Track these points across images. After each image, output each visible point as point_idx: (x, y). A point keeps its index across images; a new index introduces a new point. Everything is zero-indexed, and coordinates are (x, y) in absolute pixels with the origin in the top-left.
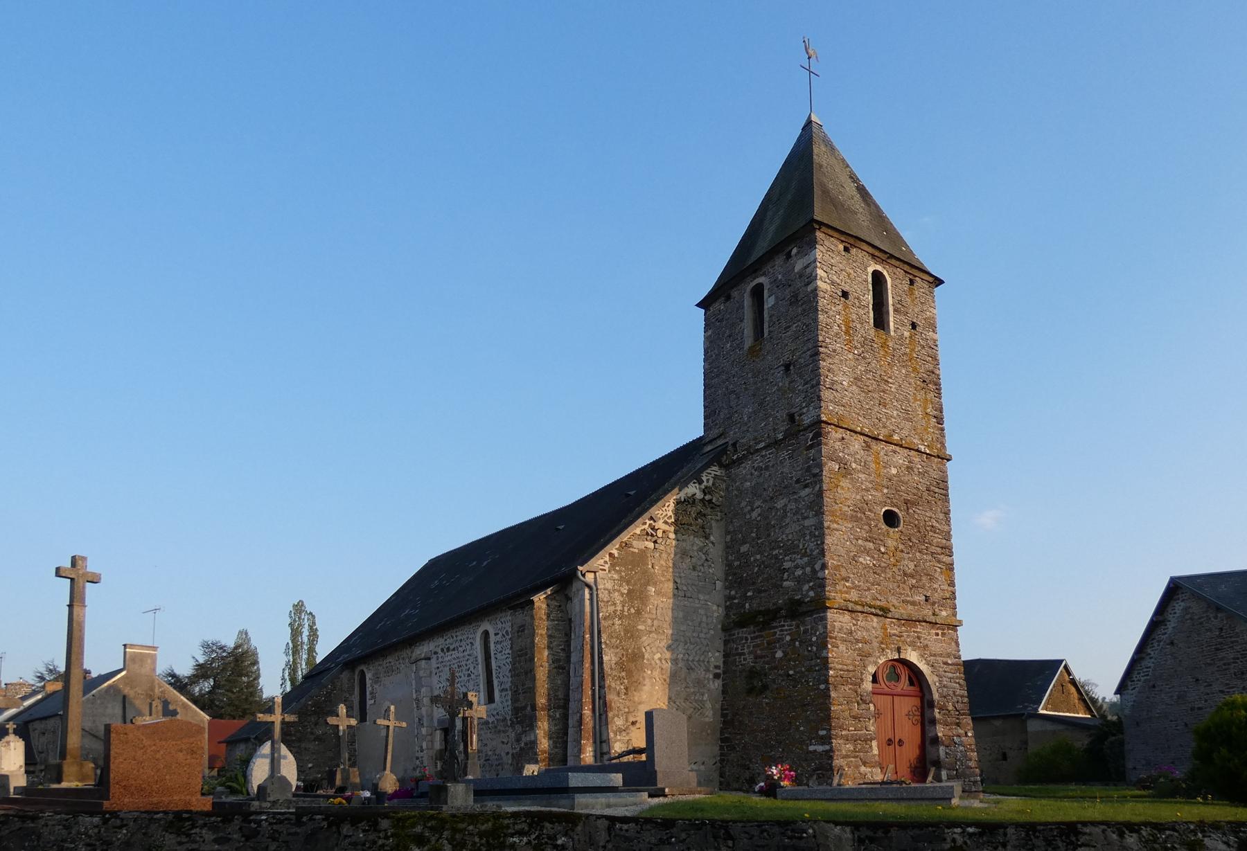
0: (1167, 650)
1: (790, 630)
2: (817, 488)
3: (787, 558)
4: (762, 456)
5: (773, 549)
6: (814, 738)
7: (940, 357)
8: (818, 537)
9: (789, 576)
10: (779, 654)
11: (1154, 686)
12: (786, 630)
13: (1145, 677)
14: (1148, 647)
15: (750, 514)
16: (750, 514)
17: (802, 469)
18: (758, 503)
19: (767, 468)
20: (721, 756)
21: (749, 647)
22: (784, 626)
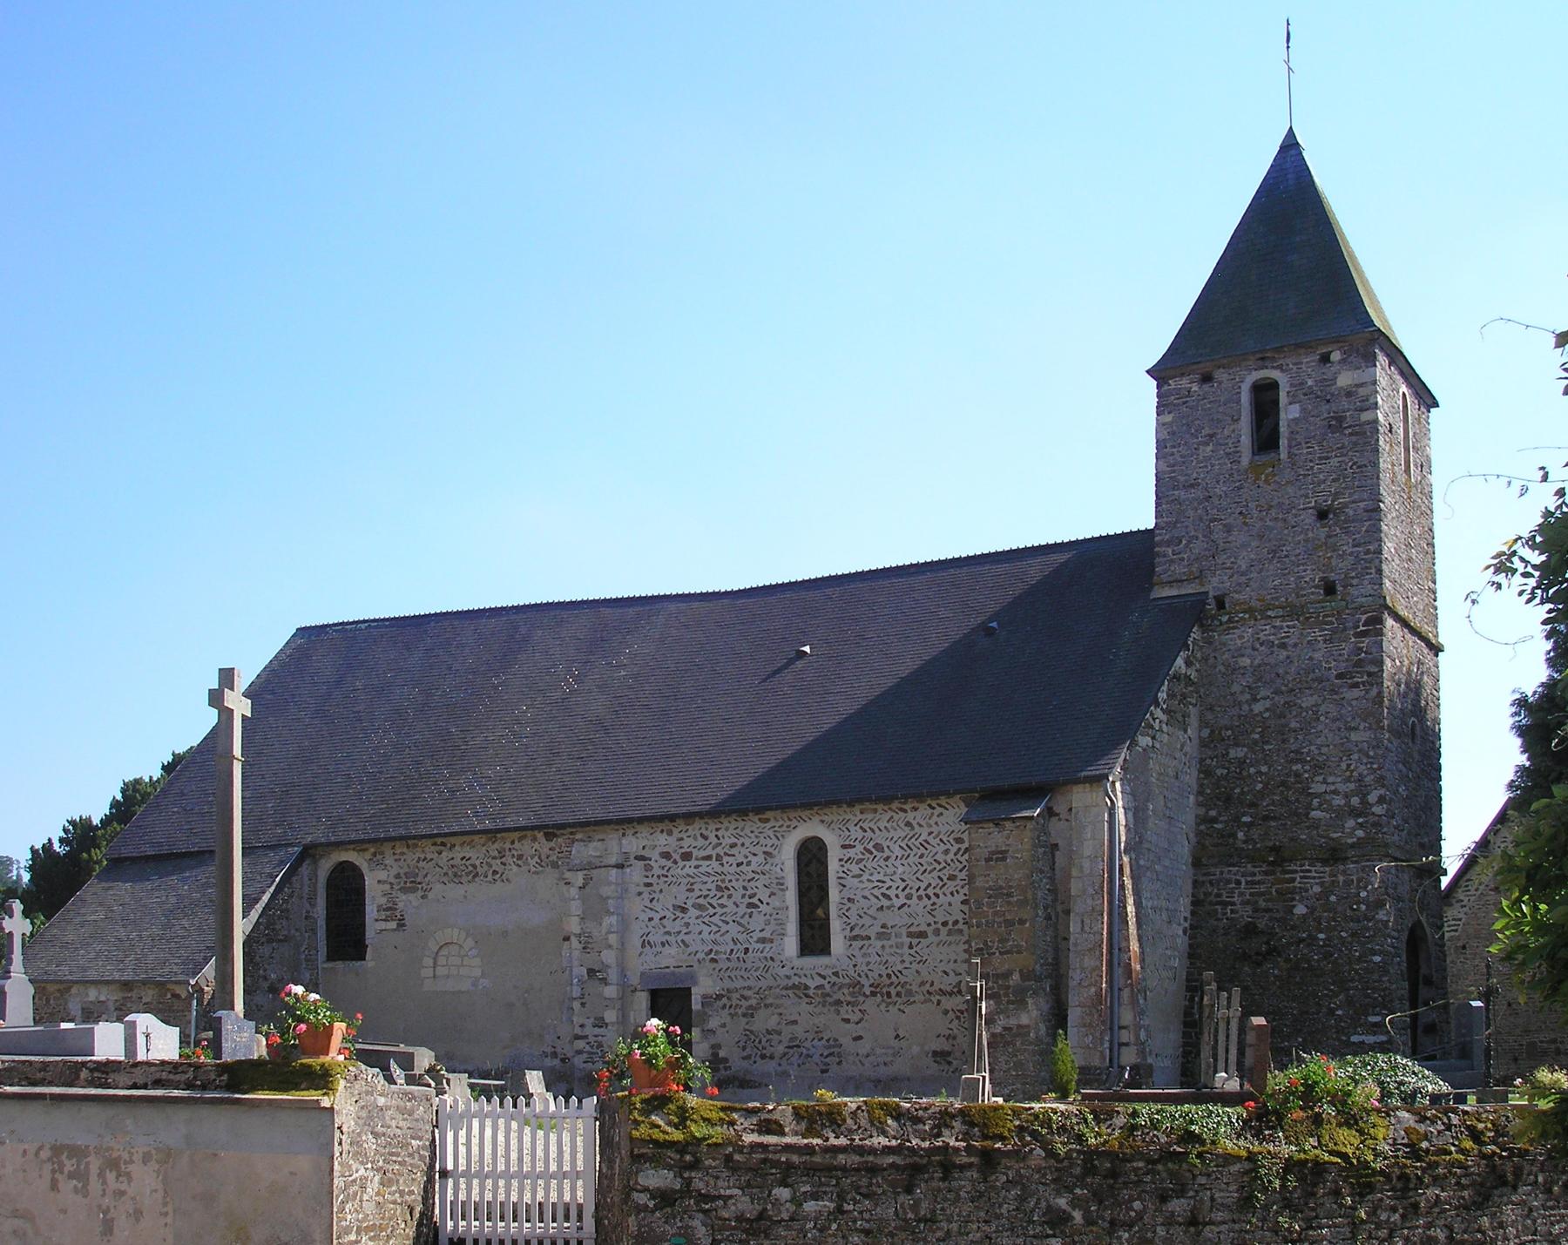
0: (1488, 898)
1: (1320, 878)
2: (1374, 692)
3: (1317, 779)
4: (1274, 627)
5: (1292, 761)
6: (1361, 1026)
7: (1434, 510)
8: (1372, 757)
9: (1321, 804)
10: (1300, 910)
11: (1464, 947)
12: (1314, 878)
13: (1453, 934)
14: (1460, 891)
15: (1250, 705)
16: (1250, 705)
17: (1347, 660)
18: (1263, 693)
19: (1283, 646)
20: (1183, 1046)
21: (1241, 894)
22: (1310, 871)
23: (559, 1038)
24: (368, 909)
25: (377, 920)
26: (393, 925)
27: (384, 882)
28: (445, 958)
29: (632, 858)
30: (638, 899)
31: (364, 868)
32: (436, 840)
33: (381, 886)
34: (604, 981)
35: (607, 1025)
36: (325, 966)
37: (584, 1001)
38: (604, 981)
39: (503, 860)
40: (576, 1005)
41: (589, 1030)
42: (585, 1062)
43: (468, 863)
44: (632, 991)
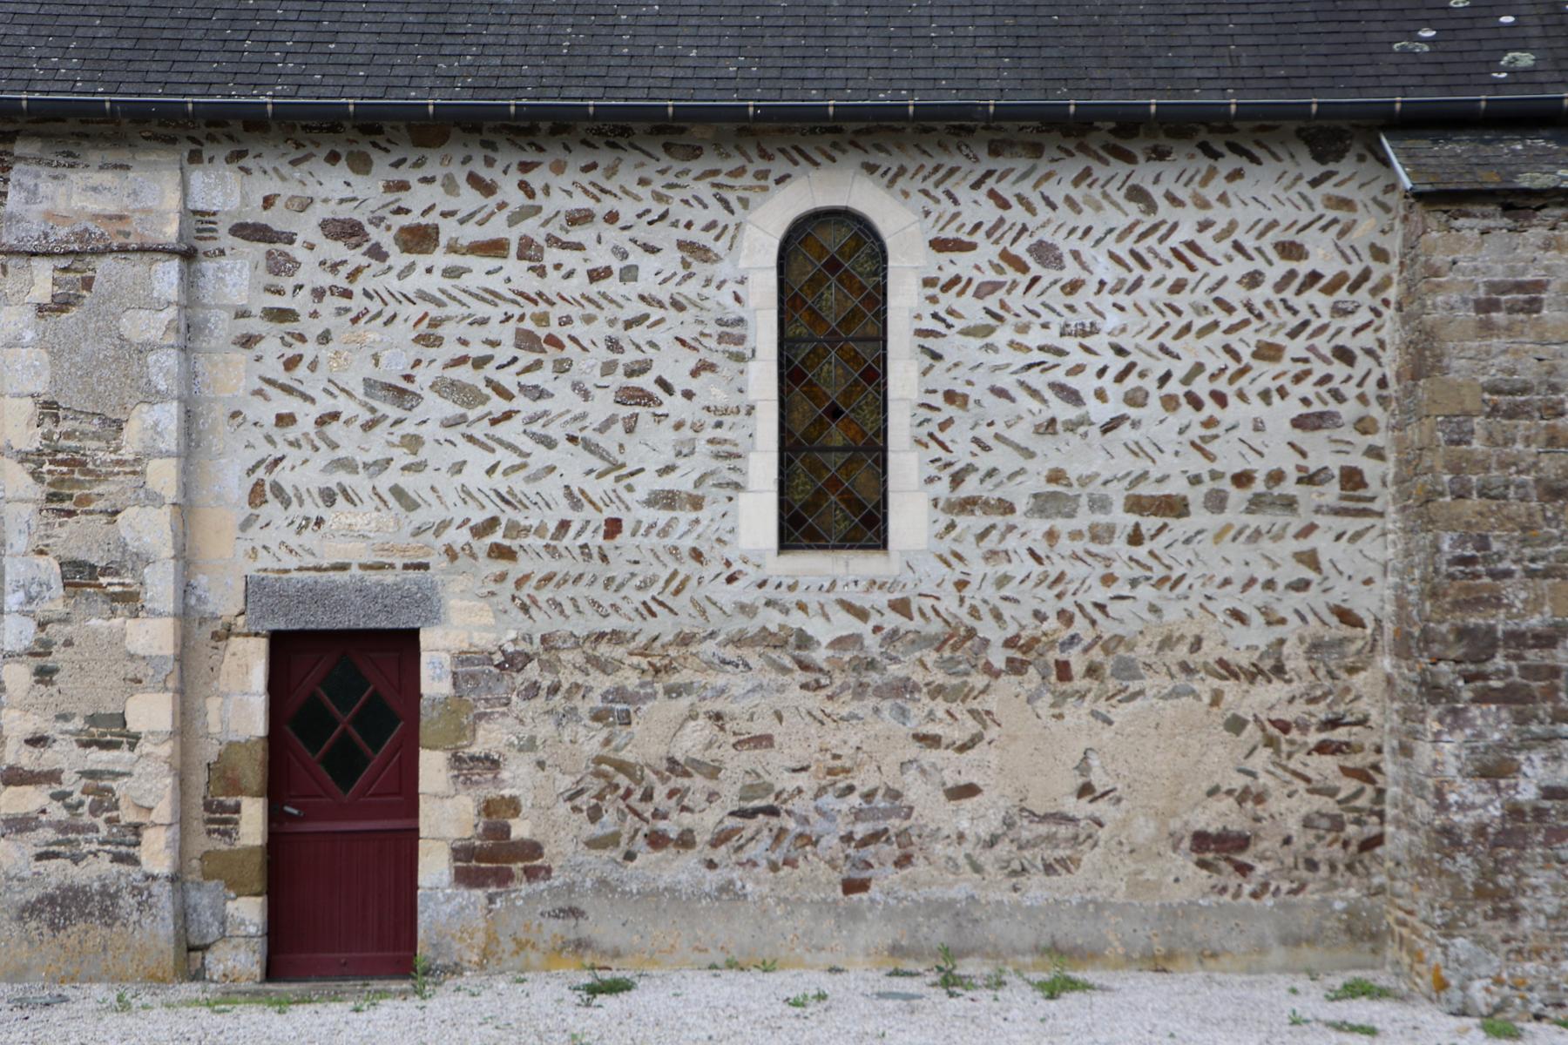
34: (129, 600)
37: (49, 662)
38: (129, 600)
41: (66, 756)
44: (215, 636)
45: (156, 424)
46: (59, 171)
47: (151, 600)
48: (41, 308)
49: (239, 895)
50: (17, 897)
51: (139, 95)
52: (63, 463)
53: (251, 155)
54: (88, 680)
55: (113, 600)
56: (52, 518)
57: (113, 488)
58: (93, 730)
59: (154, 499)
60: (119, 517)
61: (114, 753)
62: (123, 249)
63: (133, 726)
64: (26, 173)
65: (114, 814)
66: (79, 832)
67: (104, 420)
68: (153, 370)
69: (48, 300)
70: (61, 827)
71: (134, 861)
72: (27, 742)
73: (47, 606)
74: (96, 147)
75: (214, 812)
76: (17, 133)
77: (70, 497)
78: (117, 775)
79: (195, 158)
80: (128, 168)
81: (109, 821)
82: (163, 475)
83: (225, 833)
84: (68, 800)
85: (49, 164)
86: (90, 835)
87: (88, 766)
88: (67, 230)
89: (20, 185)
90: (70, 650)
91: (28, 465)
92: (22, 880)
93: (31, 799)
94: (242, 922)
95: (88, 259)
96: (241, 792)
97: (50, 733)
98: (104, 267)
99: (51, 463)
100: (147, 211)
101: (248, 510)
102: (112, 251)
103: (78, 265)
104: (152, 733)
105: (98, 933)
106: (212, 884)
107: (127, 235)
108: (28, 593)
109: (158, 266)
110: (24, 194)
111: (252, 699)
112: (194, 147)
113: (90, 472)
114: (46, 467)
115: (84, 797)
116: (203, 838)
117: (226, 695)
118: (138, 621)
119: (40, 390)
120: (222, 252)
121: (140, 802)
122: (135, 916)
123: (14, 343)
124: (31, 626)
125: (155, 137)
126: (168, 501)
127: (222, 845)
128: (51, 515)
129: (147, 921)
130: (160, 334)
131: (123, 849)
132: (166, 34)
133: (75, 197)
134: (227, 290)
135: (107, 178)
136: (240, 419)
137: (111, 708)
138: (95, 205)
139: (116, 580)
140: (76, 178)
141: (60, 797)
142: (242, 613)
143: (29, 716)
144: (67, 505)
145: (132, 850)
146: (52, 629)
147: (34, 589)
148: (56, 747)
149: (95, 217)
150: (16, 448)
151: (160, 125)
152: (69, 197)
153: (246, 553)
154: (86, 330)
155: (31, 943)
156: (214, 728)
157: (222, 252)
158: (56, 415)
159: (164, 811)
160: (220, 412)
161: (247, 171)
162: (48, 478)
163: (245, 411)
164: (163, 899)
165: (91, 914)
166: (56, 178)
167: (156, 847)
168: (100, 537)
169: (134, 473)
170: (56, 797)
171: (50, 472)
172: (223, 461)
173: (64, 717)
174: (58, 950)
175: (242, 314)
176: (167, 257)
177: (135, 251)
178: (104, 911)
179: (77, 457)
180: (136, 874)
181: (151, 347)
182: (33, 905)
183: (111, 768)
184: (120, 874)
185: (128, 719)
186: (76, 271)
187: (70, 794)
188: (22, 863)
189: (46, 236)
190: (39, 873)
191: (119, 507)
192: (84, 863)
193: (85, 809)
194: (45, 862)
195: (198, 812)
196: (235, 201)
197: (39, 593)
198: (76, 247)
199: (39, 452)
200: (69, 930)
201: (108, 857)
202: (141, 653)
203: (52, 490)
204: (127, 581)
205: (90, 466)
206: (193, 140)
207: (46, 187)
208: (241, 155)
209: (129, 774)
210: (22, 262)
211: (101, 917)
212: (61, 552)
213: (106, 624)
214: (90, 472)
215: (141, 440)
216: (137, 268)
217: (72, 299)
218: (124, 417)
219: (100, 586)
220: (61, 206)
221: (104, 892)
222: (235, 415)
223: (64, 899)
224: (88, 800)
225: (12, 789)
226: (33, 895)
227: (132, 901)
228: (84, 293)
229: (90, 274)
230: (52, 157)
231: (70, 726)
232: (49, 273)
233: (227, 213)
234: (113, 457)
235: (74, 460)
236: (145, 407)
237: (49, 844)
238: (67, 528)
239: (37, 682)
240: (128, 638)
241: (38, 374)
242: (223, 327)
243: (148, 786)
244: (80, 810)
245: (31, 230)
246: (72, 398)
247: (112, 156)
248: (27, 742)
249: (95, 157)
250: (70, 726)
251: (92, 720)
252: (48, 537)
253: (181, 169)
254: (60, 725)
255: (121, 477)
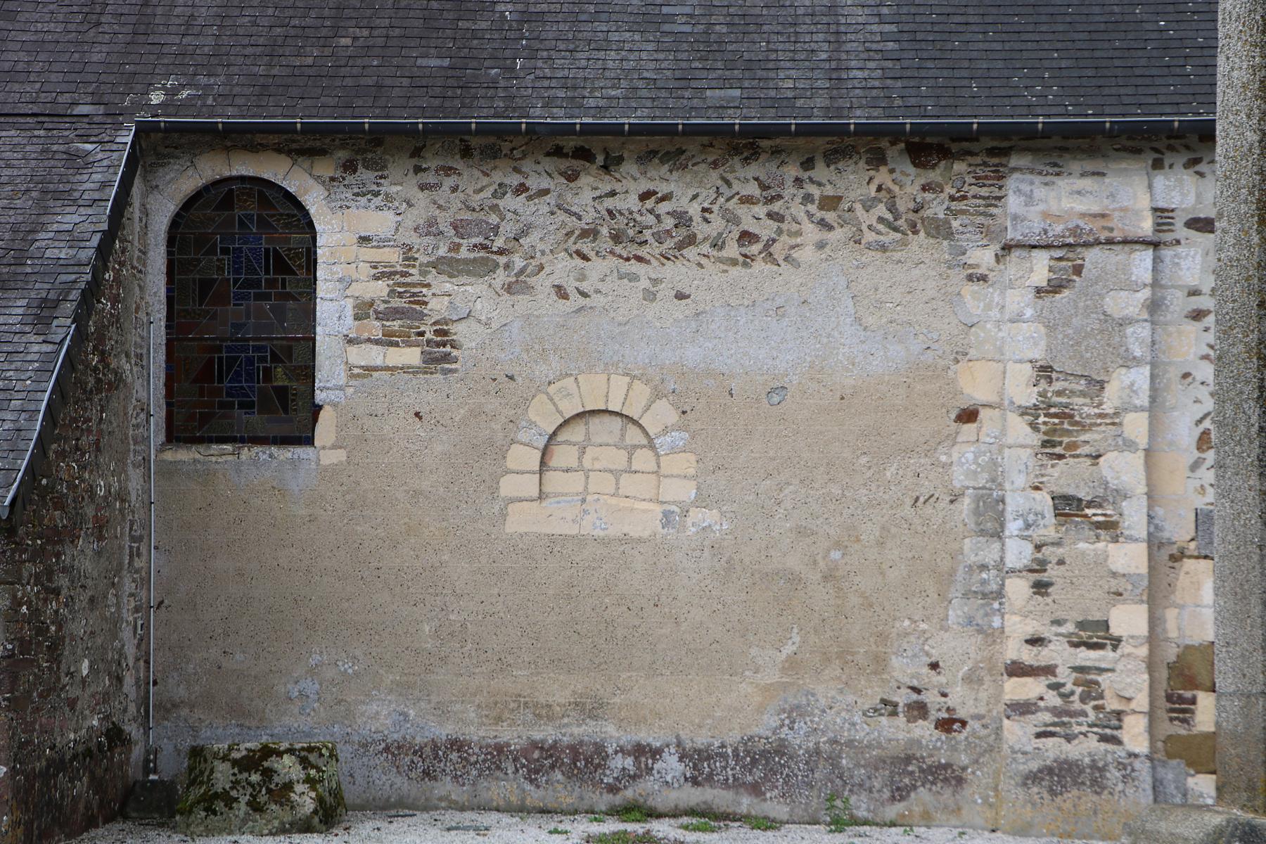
23: (934, 666)
24: (324, 310)
25: (351, 341)
26: (411, 356)
27: (383, 243)
28: (574, 451)
29: (1179, 223)
30: (1193, 328)
31: (314, 200)
32: (561, 141)
33: (369, 254)
34: (1110, 527)
35: (1116, 642)
36: (169, 456)
37: (1044, 577)
38: (1110, 527)
39: (776, 207)
40: (1018, 589)
41: (1059, 654)
42: (1039, 735)
43: (664, 208)
44: (1173, 558)
45: (1132, 384)
46: (1049, 178)
47: (1129, 528)
48: (1039, 291)
49: (1198, 772)
50: (1021, 767)
51: (1124, 115)
52: (1055, 415)
53: (1206, 160)
54: (1077, 593)
55: (1097, 528)
56: (1045, 461)
57: (1096, 436)
58: (1082, 633)
59: (1130, 445)
60: (1101, 460)
61: (1100, 653)
62: (1110, 242)
63: (1115, 630)
64: (1022, 181)
65: (1100, 702)
66: (1071, 717)
67: (1089, 380)
68: (1131, 340)
69: (1045, 284)
70: (1055, 711)
71: (1116, 741)
72: (1027, 641)
73: (1042, 531)
74: (1075, 158)
75: (1174, 703)
76: (1011, 148)
77: (1060, 443)
78: (1101, 671)
79: (1158, 165)
80: (1104, 175)
81: (1096, 708)
82: (1136, 426)
83: (1184, 721)
84: (1062, 690)
85: (1040, 173)
86: (1081, 719)
87: (1078, 663)
88: (1061, 227)
89: (1019, 191)
90: (1062, 567)
91: (1027, 417)
92: (1025, 753)
93: (1030, 688)
94: (1201, 795)
95: (1079, 250)
96: (1197, 687)
97: (1046, 635)
98: (1092, 257)
99: (1046, 415)
100: (1124, 209)
101: (1196, 454)
102: (1101, 243)
103: (1071, 255)
104: (1132, 637)
105: (1089, 799)
106: (1174, 762)
107: (1111, 230)
108: (1026, 521)
109: (1137, 255)
110: (1022, 198)
111: (1204, 610)
112: (1157, 156)
113: (1077, 423)
114: (1042, 419)
115: (1075, 688)
116: (1167, 724)
117: (1181, 607)
118: (1118, 545)
119: (1037, 357)
120: (1178, 242)
121: (1122, 694)
122: (1120, 786)
123: (1017, 319)
124: (1028, 549)
125: (1125, 149)
126: (1142, 447)
127: (1180, 730)
128: (1045, 458)
129: (1130, 791)
130: (1137, 310)
131: (1108, 731)
132: (1117, 63)
133: (1064, 200)
134: (1181, 273)
135: (1087, 183)
136: (1190, 379)
137: (1097, 616)
138: (1081, 205)
139: (1099, 511)
140: (1063, 184)
141: (1055, 687)
142: (1192, 540)
143: (1028, 621)
144: (1058, 450)
145: (1115, 733)
146: (1046, 551)
147: (1031, 518)
148: (1051, 646)
149: (1083, 215)
150: (1018, 403)
151: (1129, 138)
152: (1060, 200)
153: (1196, 490)
154: (1076, 307)
155: (1034, 804)
156: (1173, 634)
157: (1178, 242)
158: (1050, 377)
159: (1142, 701)
160: (1174, 374)
161: (1201, 175)
162: (1043, 428)
163: (1194, 373)
164: (1144, 773)
165: (1083, 783)
166: (1046, 184)
167: (1136, 730)
168: (1086, 475)
169: (1113, 424)
170: (1051, 687)
171: (1045, 423)
172: (1175, 414)
173: (1058, 622)
174: (1056, 812)
175: (1194, 293)
176: (1144, 247)
177: (1119, 243)
178: (1094, 782)
179: (1067, 411)
180: (1120, 752)
181: (1128, 321)
182: (1035, 775)
183: (1097, 664)
184: (1106, 751)
185: (1111, 624)
186: (1068, 260)
187: (1063, 685)
188: (1024, 740)
189: (1046, 232)
190: (1038, 749)
191: (1102, 451)
192: (1076, 741)
193: (1076, 698)
194: (1043, 740)
195: (1163, 703)
196: (1191, 200)
197: (1035, 521)
198: (1071, 240)
199: (1036, 407)
200: (1065, 795)
201: (1096, 737)
202: (1121, 571)
203: (1046, 438)
204: (1109, 512)
205: (1077, 418)
206: (1156, 150)
207: (1040, 192)
208: (1196, 161)
209: (1112, 670)
210: (1024, 253)
211: (1092, 786)
212: (1054, 489)
213: (1092, 547)
214: (1077, 423)
215: (1120, 397)
216: (1119, 257)
217: (1064, 283)
218: (1106, 379)
219: (1086, 516)
220: (1054, 207)
221: (1094, 765)
222: (1186, 375)
223: (1060, 770)
224: (1079, 690)
225: (1015, 679)
226: (1034, 766)
227: (1118, 774)
228: (1075, 277)
229: (1079, 262)
230: (1041, 167)
231: (1062, 630)
232: (1046, 262)
233: (1183, 210)
234: (1096, 411)
235: (1065, 413)
236: (1123, 370)
237: (1046, 725)
238: (1058, 469)
239: (1035, 593)
240: (1110, 560)
241: (1036, 344)
242: (1178, 303)
243: (1129, 680)
244: (1072, 699)
245: (1033, 227)
246: (1063, 363)
247: (1090, 166)
248: (1027, 641)
249: (1076, 166)
250: (1062, 630)
251: (1081, 625)
252: (1042, 475)
253: (1147, 174)
254: (1055, 629)
255: (1103, 428)
